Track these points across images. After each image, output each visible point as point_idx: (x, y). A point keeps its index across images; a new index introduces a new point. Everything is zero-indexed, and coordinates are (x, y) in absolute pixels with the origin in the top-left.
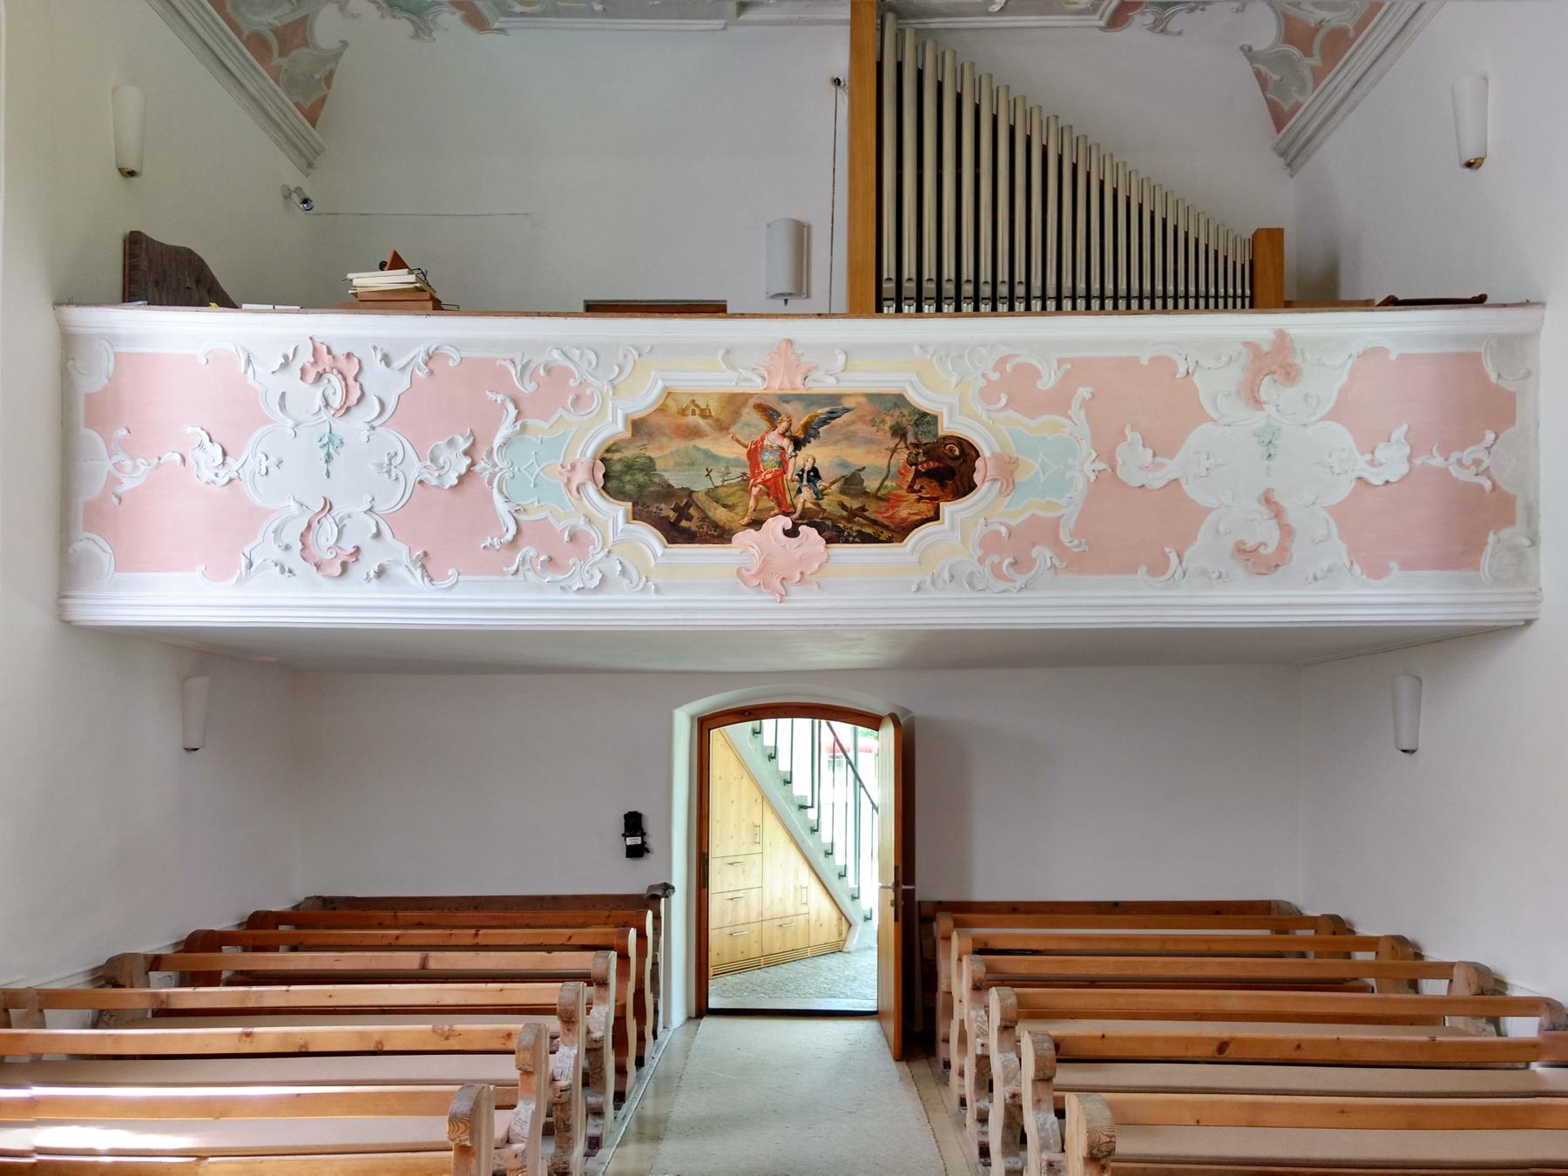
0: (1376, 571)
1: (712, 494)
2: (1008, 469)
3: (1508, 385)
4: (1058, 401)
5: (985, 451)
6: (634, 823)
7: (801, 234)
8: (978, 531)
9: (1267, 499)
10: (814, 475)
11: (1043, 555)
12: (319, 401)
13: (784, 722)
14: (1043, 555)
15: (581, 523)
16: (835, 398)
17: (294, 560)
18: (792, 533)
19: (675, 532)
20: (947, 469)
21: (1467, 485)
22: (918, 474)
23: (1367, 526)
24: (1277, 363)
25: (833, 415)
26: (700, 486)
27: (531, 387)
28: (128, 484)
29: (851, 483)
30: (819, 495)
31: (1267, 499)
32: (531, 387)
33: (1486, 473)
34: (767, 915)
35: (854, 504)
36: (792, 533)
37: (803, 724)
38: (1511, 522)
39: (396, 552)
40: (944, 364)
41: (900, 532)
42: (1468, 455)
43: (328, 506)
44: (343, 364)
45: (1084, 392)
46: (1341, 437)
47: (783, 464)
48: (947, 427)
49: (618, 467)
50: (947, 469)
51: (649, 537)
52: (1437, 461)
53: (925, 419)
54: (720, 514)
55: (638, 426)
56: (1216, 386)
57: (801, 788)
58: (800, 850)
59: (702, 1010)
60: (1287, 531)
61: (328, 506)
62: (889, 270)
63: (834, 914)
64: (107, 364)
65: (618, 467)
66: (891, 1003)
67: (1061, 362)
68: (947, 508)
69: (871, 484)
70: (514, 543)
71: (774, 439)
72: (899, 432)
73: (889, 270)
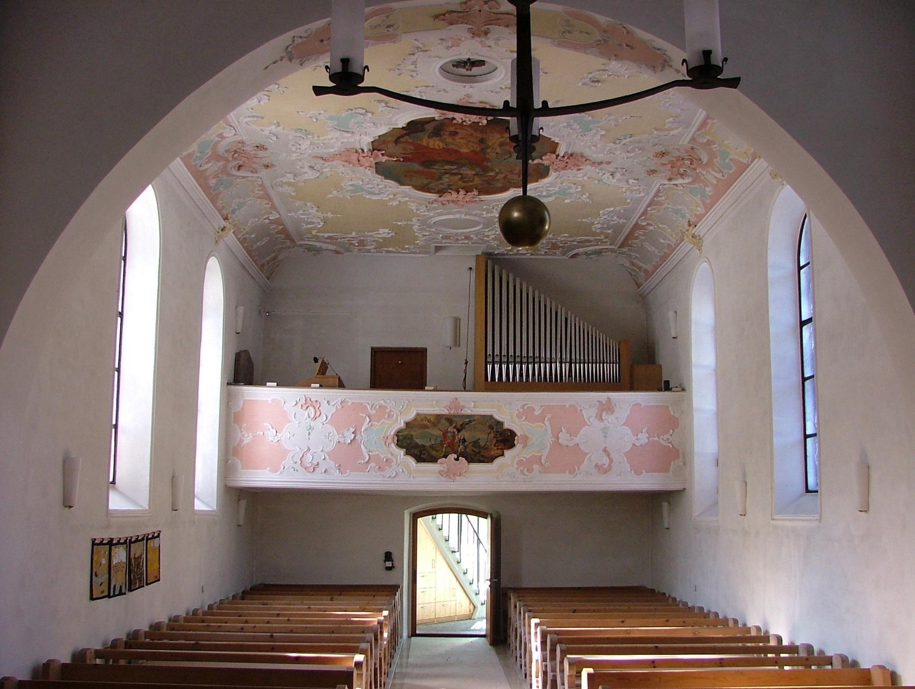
0: (638, 473)
1: (431, 447)
2: (526, 438)
3: (677, 415)
4: (542, 419)
5: (518, 434)
6: (388, 556)
7: (457, 322)
8: (517, 459)
9: (605, 450)
10: (464, 440)
11: (536, 467)
12: (306, 416)
13: (446, 516)
14: (536, 467)
15: (389, 456)
16: (471, 416)
17: (298, 467)
18: (457, 459)
19: (419, 459)
20: (506, 439)
21: (665, 447)
22: (497, 441)
23: (635, 456)
24: (608, 407)
25: (470, 422)
26: (427, 444)
27: (374, 412)
28: (247, 441)
29: (476, 443)
30: (466, 447)
31: (605, 450)
32: (374, 412)
33: (671, 443)
34: (438, 600)
35: (477, 450)
36: (457, 459)
37: (454, 516)
38: (678, 457)
39: (330, 464)
40: (504, 407)
41: (490, 460)
42: (666, 437)
43: (309, 449)
44: (314, 403)
45: (550, 416)
46: (627, 430)
47: (454, 437)
48: (506, 426)
49: (401, 438)
50: (506, 439)
51: (411, 461)
52: (656, 439)
53: (500, 424)
54: (434, 453)
55: (407, 424)
56: (589, 414)
57: (453, 543)
58: (451, 570)
59: (413, 634)
60: (611, 461)
61: (309, 449)
62: (490, 352)
63: (468, 601)
64: (241, 404)
65: (401, 438)
66: (489, 633)
67: (542, 406)
68: (506, 452)
69: (482, 444)
70: (368, 462)
71: (451, 429)
72: (491, 427)
73: (490, 352)
